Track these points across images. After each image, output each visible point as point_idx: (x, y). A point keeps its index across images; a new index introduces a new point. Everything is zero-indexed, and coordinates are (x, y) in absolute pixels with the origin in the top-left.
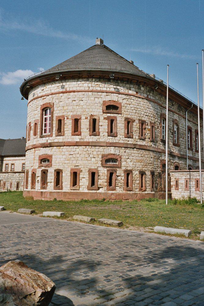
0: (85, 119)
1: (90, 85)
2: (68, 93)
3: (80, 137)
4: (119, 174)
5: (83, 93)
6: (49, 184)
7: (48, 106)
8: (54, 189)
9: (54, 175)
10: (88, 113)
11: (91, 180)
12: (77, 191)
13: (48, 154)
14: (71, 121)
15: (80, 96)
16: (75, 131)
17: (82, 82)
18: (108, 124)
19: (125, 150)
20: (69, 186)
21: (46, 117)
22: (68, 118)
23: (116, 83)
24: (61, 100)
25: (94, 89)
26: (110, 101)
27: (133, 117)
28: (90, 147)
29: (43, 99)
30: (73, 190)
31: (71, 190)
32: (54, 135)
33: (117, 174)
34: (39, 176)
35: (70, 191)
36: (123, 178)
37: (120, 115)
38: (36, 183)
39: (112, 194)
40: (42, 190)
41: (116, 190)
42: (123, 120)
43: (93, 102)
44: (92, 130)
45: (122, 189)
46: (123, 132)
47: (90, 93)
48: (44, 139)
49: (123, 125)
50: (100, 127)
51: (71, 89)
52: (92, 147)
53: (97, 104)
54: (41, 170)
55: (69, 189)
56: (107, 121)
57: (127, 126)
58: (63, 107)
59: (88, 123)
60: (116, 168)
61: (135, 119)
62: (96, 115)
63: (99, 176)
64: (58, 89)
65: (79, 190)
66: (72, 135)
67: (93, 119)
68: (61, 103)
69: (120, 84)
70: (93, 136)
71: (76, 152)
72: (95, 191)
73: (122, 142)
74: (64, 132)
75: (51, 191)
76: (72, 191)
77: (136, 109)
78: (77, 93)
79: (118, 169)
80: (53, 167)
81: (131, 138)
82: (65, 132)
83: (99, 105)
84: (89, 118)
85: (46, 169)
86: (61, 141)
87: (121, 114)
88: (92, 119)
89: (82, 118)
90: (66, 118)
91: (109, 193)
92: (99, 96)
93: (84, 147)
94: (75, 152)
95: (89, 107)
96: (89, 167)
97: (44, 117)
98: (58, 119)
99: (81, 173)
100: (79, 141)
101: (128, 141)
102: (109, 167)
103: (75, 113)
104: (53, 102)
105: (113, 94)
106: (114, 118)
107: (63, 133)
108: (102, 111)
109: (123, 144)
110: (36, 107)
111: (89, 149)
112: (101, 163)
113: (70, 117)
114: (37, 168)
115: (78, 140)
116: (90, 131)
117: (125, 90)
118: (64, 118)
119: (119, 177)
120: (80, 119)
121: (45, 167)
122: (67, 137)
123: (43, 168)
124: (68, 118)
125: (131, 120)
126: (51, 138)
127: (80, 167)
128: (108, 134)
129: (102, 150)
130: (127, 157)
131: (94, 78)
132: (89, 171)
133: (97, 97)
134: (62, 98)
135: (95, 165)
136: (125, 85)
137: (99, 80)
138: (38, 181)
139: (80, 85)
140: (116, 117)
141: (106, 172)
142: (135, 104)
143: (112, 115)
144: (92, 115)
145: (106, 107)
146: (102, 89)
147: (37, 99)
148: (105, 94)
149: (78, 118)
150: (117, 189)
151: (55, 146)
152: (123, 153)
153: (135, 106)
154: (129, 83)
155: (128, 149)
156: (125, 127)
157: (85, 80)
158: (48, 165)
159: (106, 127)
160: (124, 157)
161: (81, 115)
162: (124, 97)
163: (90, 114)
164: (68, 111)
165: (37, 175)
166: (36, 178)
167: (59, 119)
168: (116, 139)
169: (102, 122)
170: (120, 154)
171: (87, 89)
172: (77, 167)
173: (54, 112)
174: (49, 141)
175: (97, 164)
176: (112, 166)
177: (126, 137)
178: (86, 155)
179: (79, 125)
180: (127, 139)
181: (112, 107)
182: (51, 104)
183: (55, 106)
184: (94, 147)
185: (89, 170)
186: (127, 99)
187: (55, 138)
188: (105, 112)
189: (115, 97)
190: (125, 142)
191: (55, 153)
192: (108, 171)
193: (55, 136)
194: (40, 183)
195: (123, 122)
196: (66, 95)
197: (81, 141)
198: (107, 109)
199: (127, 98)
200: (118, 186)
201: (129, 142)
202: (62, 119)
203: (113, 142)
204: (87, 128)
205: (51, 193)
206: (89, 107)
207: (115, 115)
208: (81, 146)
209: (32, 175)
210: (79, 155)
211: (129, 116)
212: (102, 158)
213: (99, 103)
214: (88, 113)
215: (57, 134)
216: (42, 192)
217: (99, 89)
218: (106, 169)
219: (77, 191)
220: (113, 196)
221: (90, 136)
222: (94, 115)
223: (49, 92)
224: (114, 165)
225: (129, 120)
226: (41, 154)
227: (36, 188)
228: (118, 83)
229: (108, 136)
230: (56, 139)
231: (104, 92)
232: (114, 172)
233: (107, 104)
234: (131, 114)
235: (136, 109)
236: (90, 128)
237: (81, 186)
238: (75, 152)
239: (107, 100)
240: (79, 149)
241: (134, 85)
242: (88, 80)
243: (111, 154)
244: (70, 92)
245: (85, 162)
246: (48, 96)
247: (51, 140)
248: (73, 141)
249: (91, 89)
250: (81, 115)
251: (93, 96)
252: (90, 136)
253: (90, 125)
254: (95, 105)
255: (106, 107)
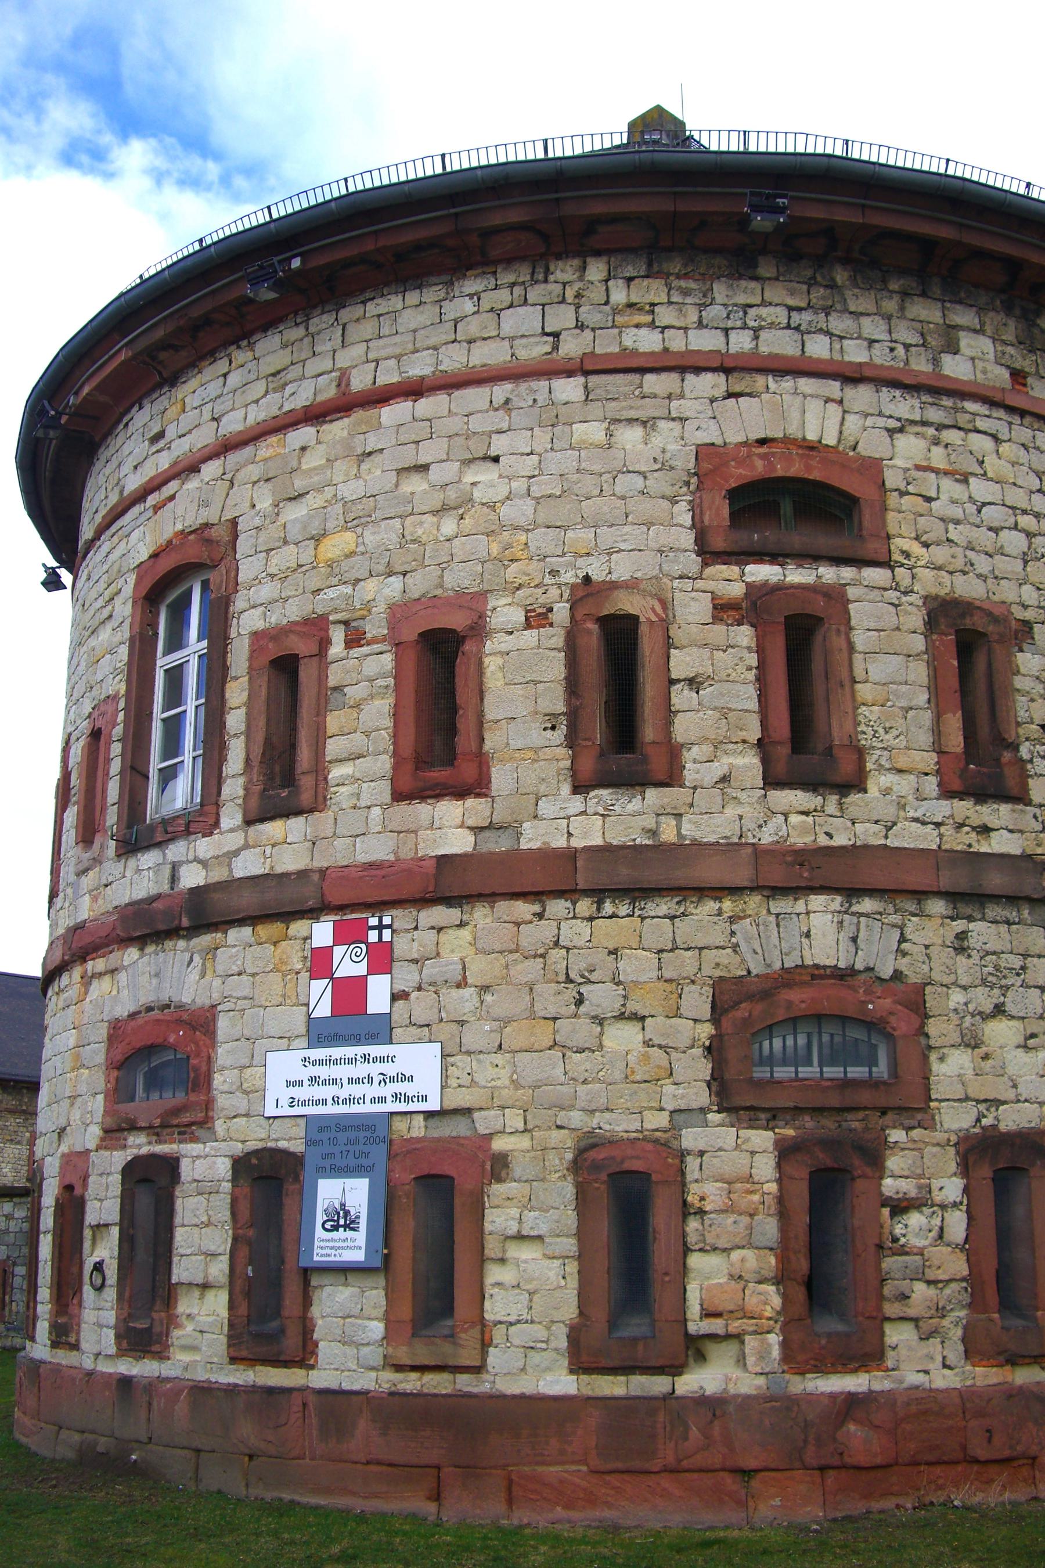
0: (528, 625)
1: (562, 318)
2: (359, 414)
3: (475, 808)
4: (908, 1187)
5: (501, 391)
6: (184, 1305)
7: (192, 553)
8: (233, 1360)
9: (226, 1215)
10: (554, 573)
11: (602, 1262)
12: (465, 1382)
13: (180, 1007)
14: (387, 661)
15: (476, 424)
16: (421, 762)
17: (489, 300)
18: (762, 667)
19: (959, 925)
20: (377, 1329)
21: (174, 659)
22: (355, 640)
23: (812, 283)
24: (299, 483)
25: (607, 345)
26: (762, 442)
27: (1007, 592)
28: (585, 906)
29: (157, 508)
30: (414, 1368)
31: (399, 1368)
32: (231, 817)
33: (889, 1186)
34: (107, 1225)
35: (388, 1380)
36: (957, 1224)
37: (874, 575)
38: (88, 1292)
39: (852, 1402)
40: (127, 1367)
41: (890, 1363)
42: (916, 619)
43: (597, 468)
44: (597, 729)
45: (955, 1352)
46: (925, 738)
47: (569, 389)
48: (148, 859)
49: (920, 672)
50: (681, 697)
51: (388, 376)
52: (608, 908)
53: (639, 482)
54: (119, 1159)
55: (374, 1355)
56: (745, 635)
57: (954, 682)
58: (317, 539)
59: (556, 668)
60: (875, 1120)
61: (1029, 615)
62: (631, 585)
63: (685, 1210)
64: (274, 398)
65: (478, 1369)
66: (398, 796)
67: (605, 621)
68: (294, 513)
69: (848, 293)
70: (604, 793)
71: (448, 964)
72: (657, 1385)
73: (926, 839)
74: (320, 769)
75: (201, 1375)
76: (411, 1383)
77: (1025, 521)
78: (442, 398)
79: (896, 1135)
80: (220, 1126)
81: (298, 813)
82: (336, 773)
83: (659, 483)
84: (561, 612)
85: (160, 1149)
86: (290, 861)
87: (887, 564)
88: (593, 627)
89: (495, 621)
90: (338, 635)
91: (811, 1398)
92: (647, 409)
93: (524, 909)
94: (431, 970)
95: (562, 512)
96: (576, 1119)
97: (163, 662)
98: (265, 660)
99: (498, 1190)
100: (468, 848)
101: (985, 830)
102: (798, 1110)
103: (419, 584)
104: (228, 515)
105: (788, 383)
106: (818, 606)
107: (306, 782)
108: (687, 539)
109: (938, 858)
110: (107, 594)
111: (575, 932)
112: (704, 1069)
113: (375, 627)
114: (91, 1145)
115: (460, 843)
116: (571, 741)
117: (907, 347)
118: (325, 643)
119: (915, 1219)
120: (479, 630)
121: (156, 1132)
122: (350, 822)
123: (139, 1145)
124: (355, 640)
125: (995, 619)
126: (204, 846)
127: (484, 1122)
128: (765, 761)
129: (717, 935)
130: (984, 999)
131: (598, 253)
132: (576, 1166)
133: (633, 414)
134: (313, 460)
135: (644, 1096)
136: (902, 309)
137: (650, 265)
138: (98, 1267)
139: (472, 327)
140: (836, 596)
141: (765, 1168)
142: (1007, 472)
143: (797, 576)
144: (587, 579)
145: (734, 495)
146: (677, 342)
147: (113, 529)
148: (710, 383)
149: (457, 621)
150: (903, 1351)
151: (241, 922)
152: (942, 956)
153: (1017, 497)
154: (937, 291)
155: (993, 911)
156: (935, 688)
157: (511, 278)
158: (177, 1111)
159: (747, 697)
160: (957, 997)
161: (483, 595)
162: (906, 407)
163: (569, 577)
164: (358, 567)
165: (91, 1217)
166: (87, 1244)
167: (274, 651)
168: (853, 811)
169: (693, 644)
170: (903, 964)
171: (535, 350)
172: (457, 1128)
173: (240, 602)
174: (192, 878)
175: (669, 1089)
176: (834, 1101)
177: (956, 785)
178: (546, 990)
179: (464, 695)
180: (964, 808)
181: (787, 507)
182: (214, 533)
183: (243, 545)
184: (624, 909)
185: (581, 1152)
186: (931, 431)
187: (236, 840)
188: (719, 543)
189: (814, 407)
190: (958, 841)
191: (241, 986)
192: (785, 1152)
193: (238, 819)
194: (111, 1294)
195: (919, 643)
196: (338, 429)
197: (484, 848)
198: (737, 517)
199: (934, 415)
200: (912, 1312)
201: (1001, 843)
202: (301, 646)
203: (823, 841)
204: (555, 715)
205: (202, 1391)
206: (562, 512)
207: (828, 574)
208: (491, 897)
209: (60, 1209)
210: (468, 992)
211: (969, 588)
212: (718, 1012)
213: (666, 467)
214: (554, 573)
215: (254, 802)
216: (125, 1383)
217: (647, 341)
218: (762, 1139)
219: (465, 1382)
220: (852, 1427)
221: (576, 789)
222: (614, 586)
223: (204, 437)
224: (846, 1084)
225: (977, 622)
226: (122, 1011)
227: (84, 1345)
228: (832, 286)
229: (772, 781)
230: (246, 846)
231: (698, 370)
232: (857, 1162)
233: (739, 474)
234: (983, 564)
235: (1025, 521)
236: (573, 717)
237: (498, 1334)
238: (431, 970)
239: (735, 437)
240: (465, 933)
241: (981, 310)
242: (541, 277)
243: (818, 974)
244: (381, 397)
245: (531, 1066)
246: (194, 469)
247: (204, 863)
248: (406, 853)
249: (572, 347)
250: (483, 595)
251: (596, 409)
252: (576, 789)
253: (573, 685)
254: (619, 489)
255: (734, 495)
